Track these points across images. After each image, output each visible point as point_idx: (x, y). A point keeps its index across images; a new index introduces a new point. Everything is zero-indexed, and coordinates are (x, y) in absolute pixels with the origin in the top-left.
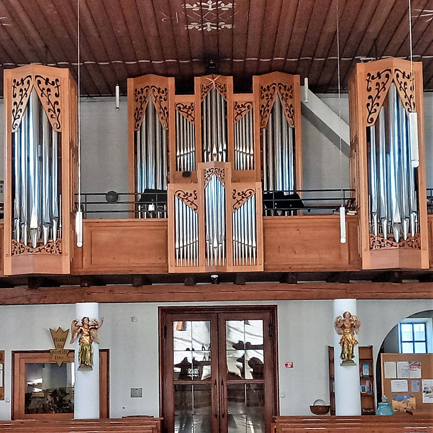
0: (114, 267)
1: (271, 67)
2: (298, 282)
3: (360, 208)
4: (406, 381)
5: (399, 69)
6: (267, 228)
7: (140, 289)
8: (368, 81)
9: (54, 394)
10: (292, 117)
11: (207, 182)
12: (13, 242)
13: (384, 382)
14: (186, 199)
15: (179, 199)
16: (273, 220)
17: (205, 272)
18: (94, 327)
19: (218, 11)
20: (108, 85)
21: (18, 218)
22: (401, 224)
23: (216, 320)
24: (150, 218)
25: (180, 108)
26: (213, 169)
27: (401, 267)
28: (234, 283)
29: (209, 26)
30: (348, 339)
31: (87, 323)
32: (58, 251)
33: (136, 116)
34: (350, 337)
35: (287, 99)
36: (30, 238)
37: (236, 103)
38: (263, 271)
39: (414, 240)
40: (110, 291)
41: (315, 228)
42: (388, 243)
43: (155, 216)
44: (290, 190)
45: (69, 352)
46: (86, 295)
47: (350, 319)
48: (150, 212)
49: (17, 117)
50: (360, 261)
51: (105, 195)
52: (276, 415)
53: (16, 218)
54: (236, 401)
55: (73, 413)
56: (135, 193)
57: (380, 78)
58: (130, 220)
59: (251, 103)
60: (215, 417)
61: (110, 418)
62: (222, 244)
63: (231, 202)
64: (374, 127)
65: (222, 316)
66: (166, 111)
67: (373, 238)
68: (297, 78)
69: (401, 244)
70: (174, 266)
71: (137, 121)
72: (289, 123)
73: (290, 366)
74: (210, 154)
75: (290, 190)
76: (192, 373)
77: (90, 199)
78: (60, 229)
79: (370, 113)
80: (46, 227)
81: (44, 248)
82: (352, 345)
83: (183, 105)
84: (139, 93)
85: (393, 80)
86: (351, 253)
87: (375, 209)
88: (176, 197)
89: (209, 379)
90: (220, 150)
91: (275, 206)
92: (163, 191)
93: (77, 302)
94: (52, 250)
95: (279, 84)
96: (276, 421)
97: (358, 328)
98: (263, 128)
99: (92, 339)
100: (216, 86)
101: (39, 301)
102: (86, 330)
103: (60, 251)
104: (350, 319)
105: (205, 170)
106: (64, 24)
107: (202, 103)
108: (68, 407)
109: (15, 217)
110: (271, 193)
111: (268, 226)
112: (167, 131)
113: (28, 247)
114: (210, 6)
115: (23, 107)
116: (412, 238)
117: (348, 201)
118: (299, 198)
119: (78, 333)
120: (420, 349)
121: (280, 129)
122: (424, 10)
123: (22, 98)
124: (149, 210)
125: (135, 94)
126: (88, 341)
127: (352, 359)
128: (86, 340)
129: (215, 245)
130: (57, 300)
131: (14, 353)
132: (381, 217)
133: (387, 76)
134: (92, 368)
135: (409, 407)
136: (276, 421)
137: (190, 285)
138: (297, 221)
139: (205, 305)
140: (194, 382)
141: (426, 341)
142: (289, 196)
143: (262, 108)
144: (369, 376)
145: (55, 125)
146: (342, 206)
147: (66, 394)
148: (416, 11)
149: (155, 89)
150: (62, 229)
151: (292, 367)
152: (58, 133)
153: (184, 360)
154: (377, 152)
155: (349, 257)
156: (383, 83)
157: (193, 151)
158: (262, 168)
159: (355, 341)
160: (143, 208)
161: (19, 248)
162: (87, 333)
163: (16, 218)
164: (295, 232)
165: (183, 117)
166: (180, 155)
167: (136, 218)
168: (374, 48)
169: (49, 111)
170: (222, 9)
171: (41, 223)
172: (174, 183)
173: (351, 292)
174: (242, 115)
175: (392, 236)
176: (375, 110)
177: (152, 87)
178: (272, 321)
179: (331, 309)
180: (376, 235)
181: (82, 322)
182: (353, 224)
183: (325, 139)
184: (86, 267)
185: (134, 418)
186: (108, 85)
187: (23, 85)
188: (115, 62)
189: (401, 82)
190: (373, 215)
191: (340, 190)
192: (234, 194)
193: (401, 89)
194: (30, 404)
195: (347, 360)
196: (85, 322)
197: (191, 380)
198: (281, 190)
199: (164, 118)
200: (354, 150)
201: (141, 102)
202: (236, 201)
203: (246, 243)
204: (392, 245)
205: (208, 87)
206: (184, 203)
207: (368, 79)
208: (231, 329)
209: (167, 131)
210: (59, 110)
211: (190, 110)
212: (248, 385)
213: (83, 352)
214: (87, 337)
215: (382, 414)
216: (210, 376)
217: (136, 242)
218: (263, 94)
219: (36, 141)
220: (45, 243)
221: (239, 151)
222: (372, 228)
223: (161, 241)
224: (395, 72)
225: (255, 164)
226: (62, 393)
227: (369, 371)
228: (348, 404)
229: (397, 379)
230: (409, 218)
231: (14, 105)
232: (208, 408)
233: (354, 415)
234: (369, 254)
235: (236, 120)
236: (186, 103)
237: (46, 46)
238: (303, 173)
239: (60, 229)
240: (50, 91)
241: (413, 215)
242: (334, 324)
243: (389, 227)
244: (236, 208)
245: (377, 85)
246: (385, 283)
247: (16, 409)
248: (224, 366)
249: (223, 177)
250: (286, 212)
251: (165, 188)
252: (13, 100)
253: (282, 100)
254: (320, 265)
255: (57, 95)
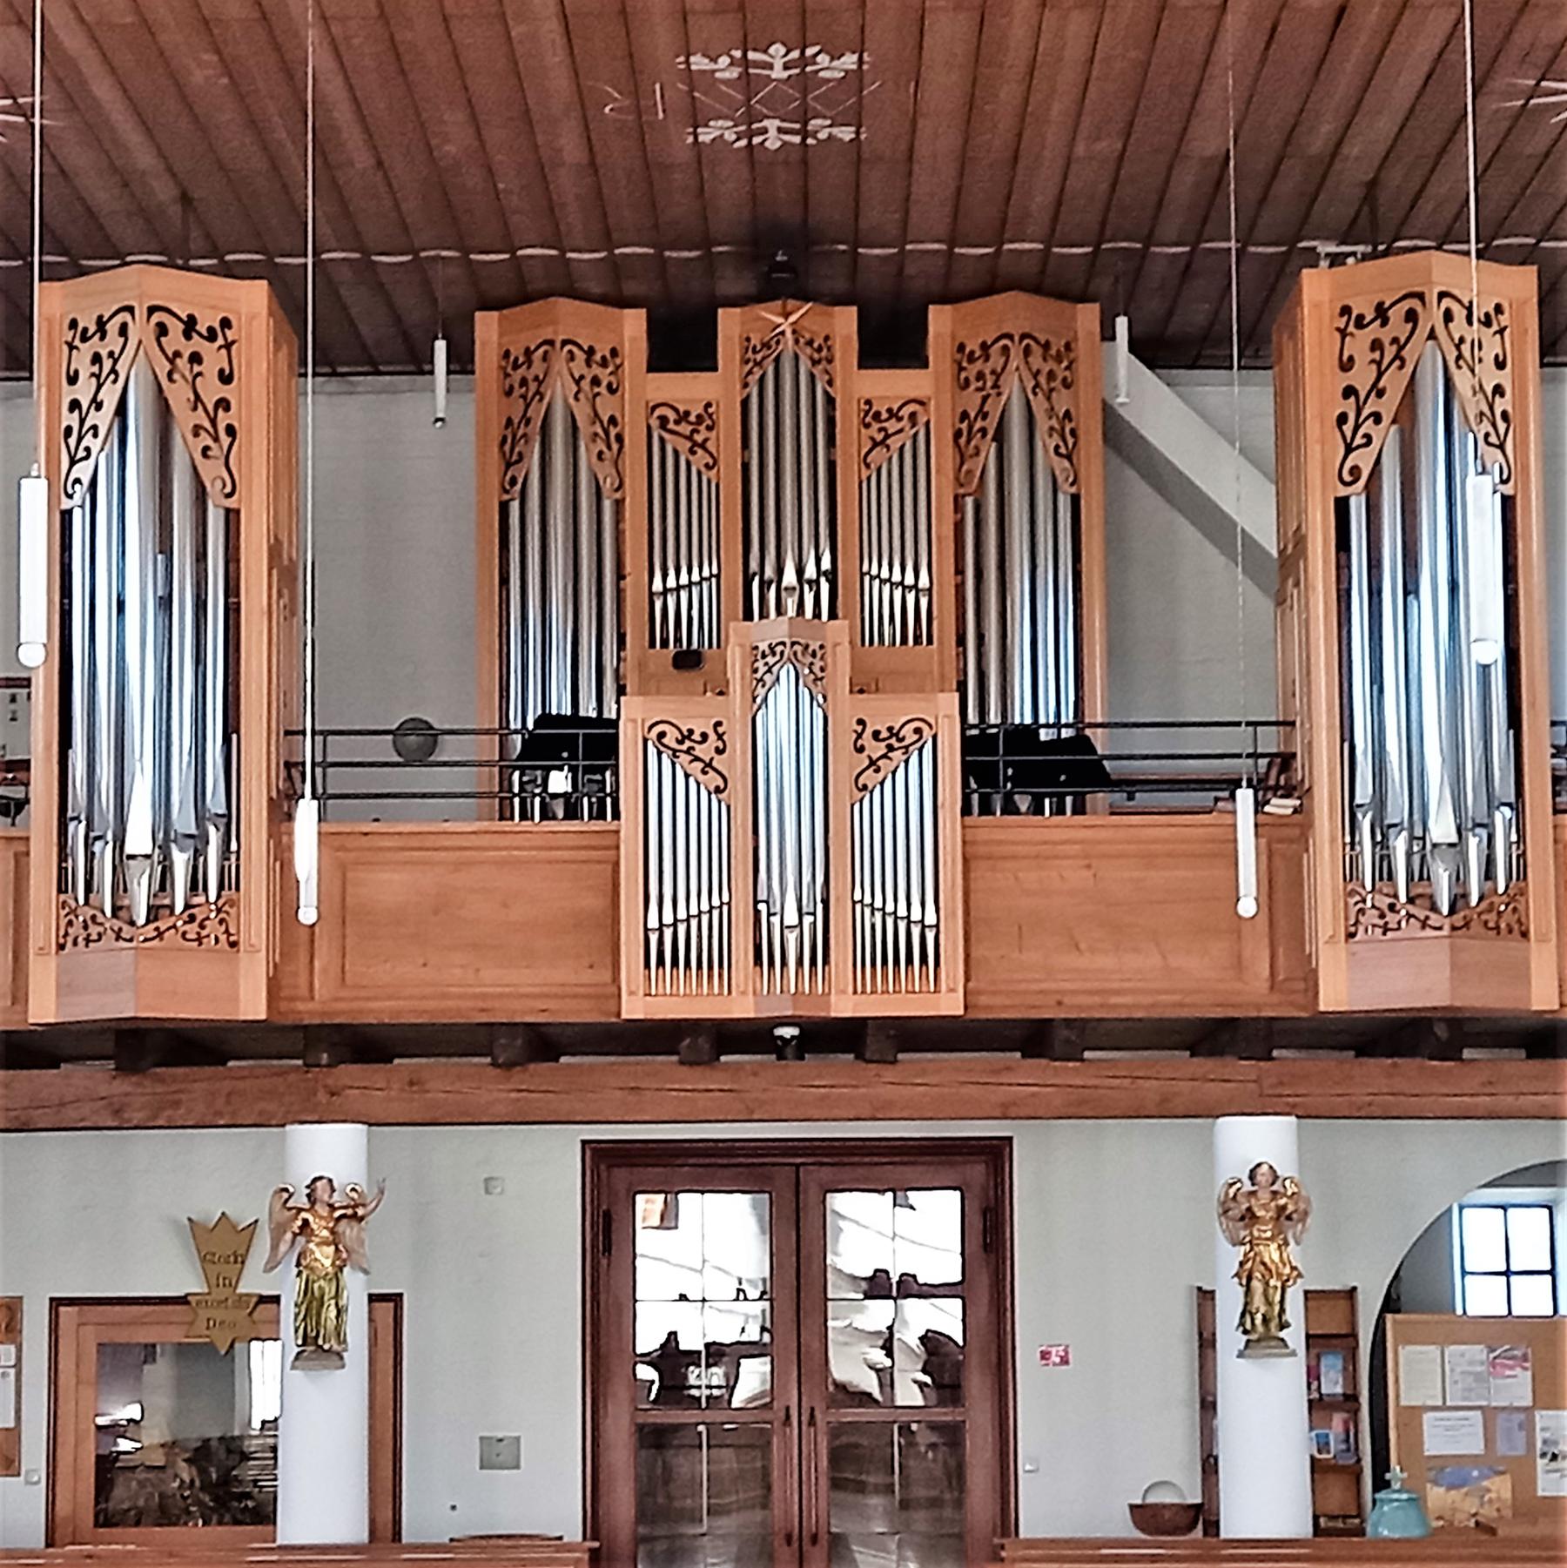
0: (424, 998)
1: (994, 276)
2: (1087, 1054)
3: (1310, 789)
4: (1479, 1413)
5: (1456, 292)
6: (976, 858)
7: (520, 1078)
8: (1343, 333)
9: (201, 1454)
10: (1069, 457)
11: (761, 691)
12: (64, 902)
13: (1398, 1415)
14: (689, 751)
15: (660, 753)
16: (997, 828)
17: (752, 1015)
18: (350, 1212)
19: (805, 81)
20: (406, 336)
21: (83, 817)
22: (1458, 846)
23: (789, 1195)
24: (554, 818)
25: (663, 420)
26: (784, 644)
27: (1458, 1004)
28: (857, 1058)
29: (772, 132)
30: (1267, 1260)
31: (326, 1198)
32: (223, 938)
33: (507, 448)
34: (1271, 1253)
35: (1052, 390)
36: (125, 890)
37: (868, 402)
38: (961, 1012)
39: (1507, 905)
40: (411, 1083)
41: (1149, 859)
42: (1409, 916)
43: (572, 813)
44: (1063, 721)
45: (257, 1304)
46: (322, 1097)
47: (1274, 1188)
48: (555, 796)
49: (81, 454)
50: (1311, 980)
51: (390, 737)
52: (1005, 1533)
53: (73, 819)
54: (861, 1488)
55: (275, 1523)
56: (501, 728)
57: (1384, 323)
58: (485, 825)
59: (922, 403)
60: (783, 1542)
61: (404, 1541)
62: (814, 914)
63: (846, 764)
64: (1363, 498)
65: (813, 1177)
66: (613, 432)
67: (1358, 898)
68: (1088, 316)
69: (1458, 919)
70: (641, 993)
71: (508, 465)
72: (1060, 480)
73: (1058, 1360)
74: (773, 587)
75: (1063, 721)
76: (704, 1382)
77: (339, 749)
78: (233, 858)
79: (1349, 449)
80: (182, 850)
81: (174, 926)
82: (1279, 1284)
83: (676, 410)
84: (516, 366)
85: (1432, 329)
86: (1281, 950)
87: (1364, 793)
88: (650, 743)
89: (765, 1403)
90: (810, 572)
91: (1006, 779)
92: (600, 721)
93: (293, 1122)
94: (204, 933)
95: (1023, 337)
96: (1004, 1554)
97: (1303, 1220)
98: (964, 496)
99: (344, 1255)
100: (797, 342)
101: (155, 1117)
102: (323, 1223)
103: (232, 939)
104: (1274, 1188)
105: (756, 648)
106: (254, 125)
107: (745, 403)
108: (250, 1504)
109: (70, 814)
110: (994, 731)
111: (982, 850)
112: (619, 505)
113: (117, 924)
114: (778, 64)
115: (103, 418)
116: (1496, 899)
117: (1270, 765)
118: (1093, 751)
119: (295, 1235)
120: (1532, 1299)
121: (1026, 496)
122: (1543, 84)
123: (99, 387)
124: (551, 790)
125: (504, 369)
126: (328, 1263)
127: (1282, 1334)
128: (324, 1257)
129: (791, 918)
130: (219, 1114)
131: (56, 1303)
132: (1387, 822)
133: (1411, 316)
134: (342, 1358)
135: (1488, 1513)
136: (1004, 1554)
137: (698, 1064)
138: (1088, 833)
139: (264, 875)
140: (710, 1416)
141: (1552, 1272)
142: (1057, 745)
143: (962, 421)
144: (1344, 1394)
145: (219, 484)
146: (1244, 783)
147: (246, 1457)
148: (1515, 85)
149: (575, 350)
150: (238, 859)
151: (1064, 1361)
152: (228, 511)
153: (668, 1340)
154: (1409, 545)
155: (1272, 966)
156: (1395, 340)
157: (712, 575)
158: (961, 641)
159: (1294, 1268)
160: (529, 782)
161: (86, 927)
162: (325, 1233)
163: (73, 819)
164: (1078, 877)
165: (676, 453)
166: (666, 591)
167: (502, 818)
168: (1366, 209)
169: (196, 435)
170: (822, 74)
171: (164, 838)
172: (640, 694)
173: (1278, 1091)
174: (888, 447)
175: (1428, 891)
176: (1368, 437)
177: (565, 343)
178: (992, 1193)
179: (1208, 1150)
180: (1369, 887)
181: (308, 1196)
182: (1285, 848)
183: (1189, 533)
184: (324, 997)
185: (492, 1542)
186: (406, 336)
187: (102, 338)
188: (432, 253)
189: (1462, 340)
190: (1360, 816)
191: (1238, 724)
192: (859, 736)
193: (1461, 362)
194: (113, 1492)
195: (1262, 1336)
196: (319, 1192)
197: (700, 1408)
198: (1028, 720)
199: (607, 454)
200: (1290, 582)
201: (524, 397)
202: (867, 763)
203: (902, 912)
204: (1424, 925)
205: (766, 345)
206: (678, 767)
207: (1342, 326)
208: (842, 1223)
209: (619, 505)
210: (231, 431)
211: (702, 428)
212: (905, 1429)
213: (311, 1304)
214: (325, 1248)
215: (1386, 1533)
216: (768, 1400)
217: (505, 905)
218: (963, 375)
219: (150, 539)
220: (179, 907)
221: (883, 582)
222: (1354, 862)
223: (595, 902)
224: (1439, 301)
225: (935, 624)
226: (229, 1451)
227: (1345, 1379)
228: (1267, 1492)
229: (1444, 1408)
230: (1489, 826)
231: (71, 410)
232: (758, 1515)
233: (1293, 1536)
234: (1343, 955)
235: (868, 466)
236: (692, 401)
237: (185, 199)
238: (1109, 664)
239: (233, 858)
240: (200, 362)
241: (1503, 816)
242: (1215, 1209)
243: (1416, 859)
244: (865, 787)
245: (1373, 349)
246: (1399, 1061)
247: (62, 1507)
248: (819, 1356)
249: (820, 675)
250: (1047, 801)
251: (610, 713)
252: (68, 394)
253: (1035, 394)
254: (1166, 992)
255: (226, 378)
